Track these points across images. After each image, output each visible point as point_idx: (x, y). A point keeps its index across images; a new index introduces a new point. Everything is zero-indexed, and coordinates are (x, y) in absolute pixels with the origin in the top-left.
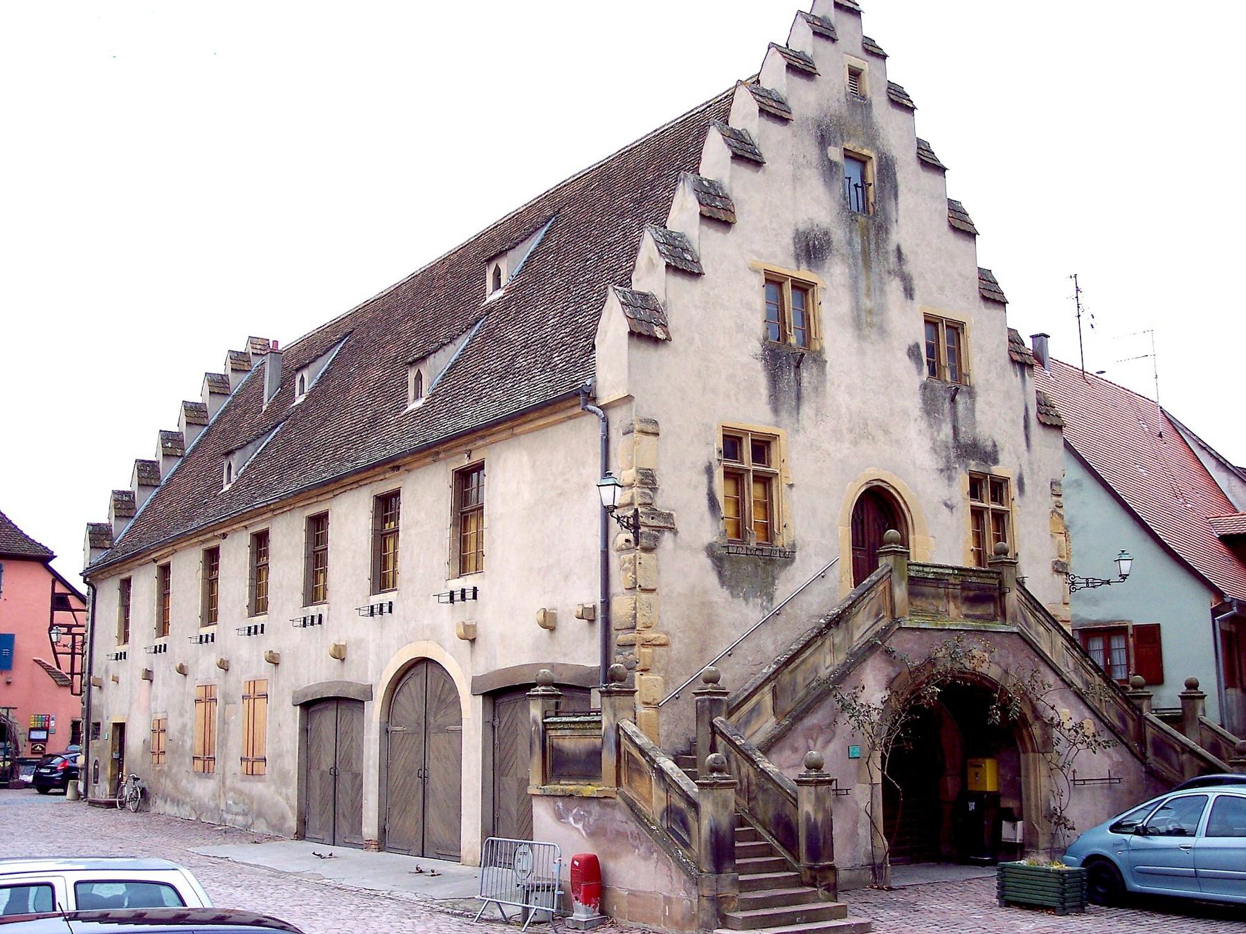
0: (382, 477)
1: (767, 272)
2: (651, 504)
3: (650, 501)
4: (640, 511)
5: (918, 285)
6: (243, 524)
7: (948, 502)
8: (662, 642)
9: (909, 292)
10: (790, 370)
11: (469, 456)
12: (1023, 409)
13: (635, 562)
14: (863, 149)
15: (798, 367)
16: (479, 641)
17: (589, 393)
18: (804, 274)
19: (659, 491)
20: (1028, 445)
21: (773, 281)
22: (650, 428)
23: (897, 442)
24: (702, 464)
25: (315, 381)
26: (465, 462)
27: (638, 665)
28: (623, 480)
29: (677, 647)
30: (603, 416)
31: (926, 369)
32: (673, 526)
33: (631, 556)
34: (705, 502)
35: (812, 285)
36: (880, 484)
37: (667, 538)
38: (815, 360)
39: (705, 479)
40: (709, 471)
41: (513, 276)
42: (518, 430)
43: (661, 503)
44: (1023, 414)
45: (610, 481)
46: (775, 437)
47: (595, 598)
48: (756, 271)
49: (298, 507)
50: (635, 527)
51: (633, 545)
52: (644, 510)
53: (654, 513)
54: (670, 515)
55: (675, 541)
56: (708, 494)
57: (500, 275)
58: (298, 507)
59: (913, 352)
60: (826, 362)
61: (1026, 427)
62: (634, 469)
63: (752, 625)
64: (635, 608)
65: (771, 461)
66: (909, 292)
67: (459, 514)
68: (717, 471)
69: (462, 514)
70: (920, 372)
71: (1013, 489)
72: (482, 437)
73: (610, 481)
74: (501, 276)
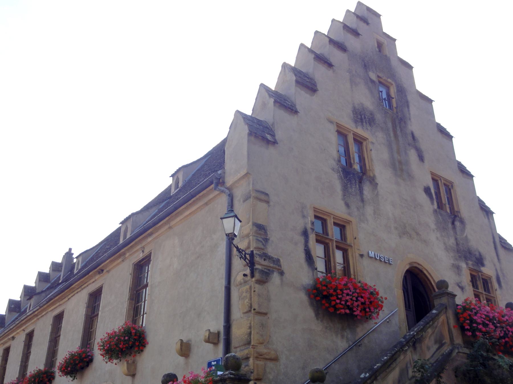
0: (93, 280)
1: (338, 125)
2: (263, 249)
3: (262, 247)
4: (255, 252)
5: (426, 156)
6: (22, 328)
7: (460, 284)
8: (273, 357)
9: (421, 158)
10: (356, 182)
11: (143, 251)
12: (492, 237)
13: (251, 290)
14: (388, 79)
15: (360, 182)
16: (138, 376)
17: (220, 179)
19: (270, 242)
20: (499, 259)
21: (342, 133)
22: (263, 197)
24: (300, 228)
25: (85, 262)
26: (141, 256)
27: (252, 375)
28: (243, 233)
29: (283, 360)
30: (229, 193)
31: (435, 203)
32: (279, 268)
33: (248, 287)
34: (302, 255)
35: (365, 139)
36: (417, 266)
37: (275, 277)
38: (371, 182)
39: (302, 239)
40: (305, 233)
41: (185, 181)
42: (173, 223)
43: (270, 251)
44: (492, 240)
45: (232, 214)
47: (218, 326)
48: (331, 122)
49: (49, 311)
50: (251, 264)
51: (249, 277)
52: (258, 252)
53: (266, 256)
54: (278, 260)
55: (282, 280)
56: (305, 250)
57: (179, 183)
58: (49, 311)
59: (427, 190)
60: (378, 184)
61: (496, 248)
62: (251, 223)
63: (341, 350)
64: (250, 328)
65: (347, 239)
66: (421, 158)
67: (135, 292)
69: (137, 291)
70: (432, 203)
72: (150, 235)
73: (232, 214)
74: (179, 184)
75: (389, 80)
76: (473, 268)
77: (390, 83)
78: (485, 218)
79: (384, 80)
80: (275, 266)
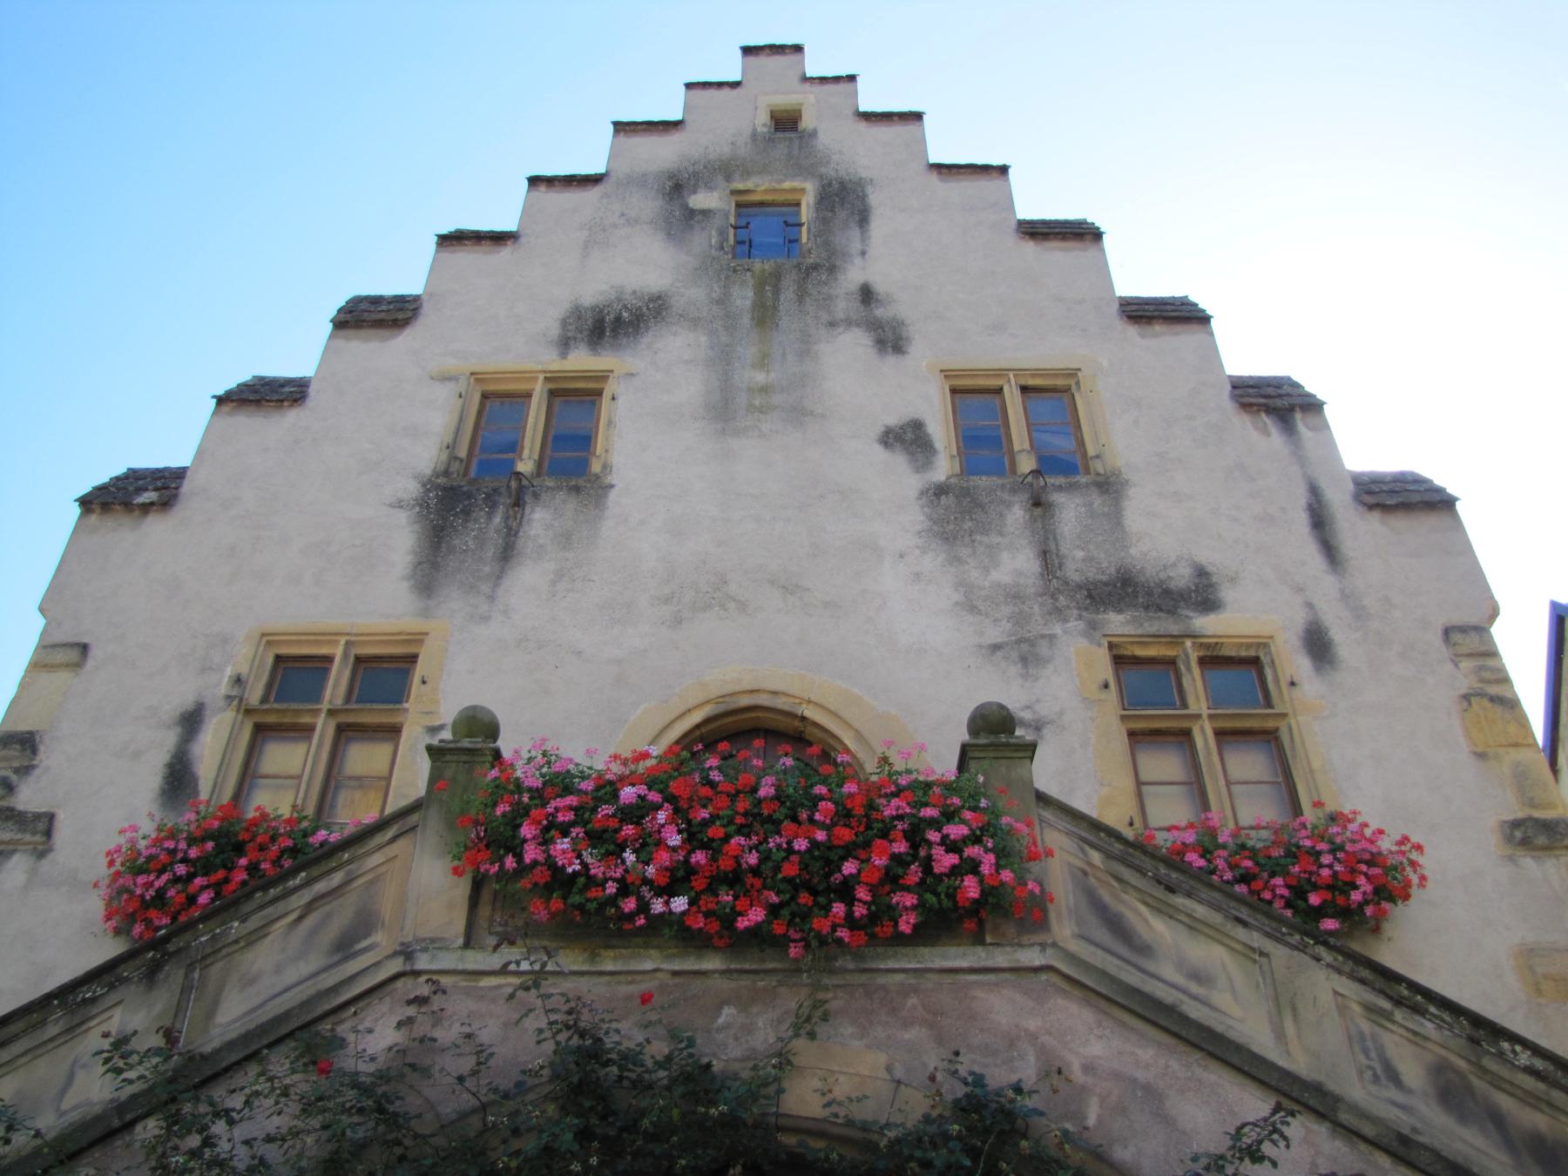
18: (582, 360)
23: (826, 605)
35: (603, 377)
39: (171, 738)
46: (419, 638)
48: (446, 378)
68: (214, 720)
71: (1292, 661)
75: (787, 185)
76: (1140, 632)
77: (793, 190)
78: (1267, 433)
79: (766, 191)
80: (19, 836)
